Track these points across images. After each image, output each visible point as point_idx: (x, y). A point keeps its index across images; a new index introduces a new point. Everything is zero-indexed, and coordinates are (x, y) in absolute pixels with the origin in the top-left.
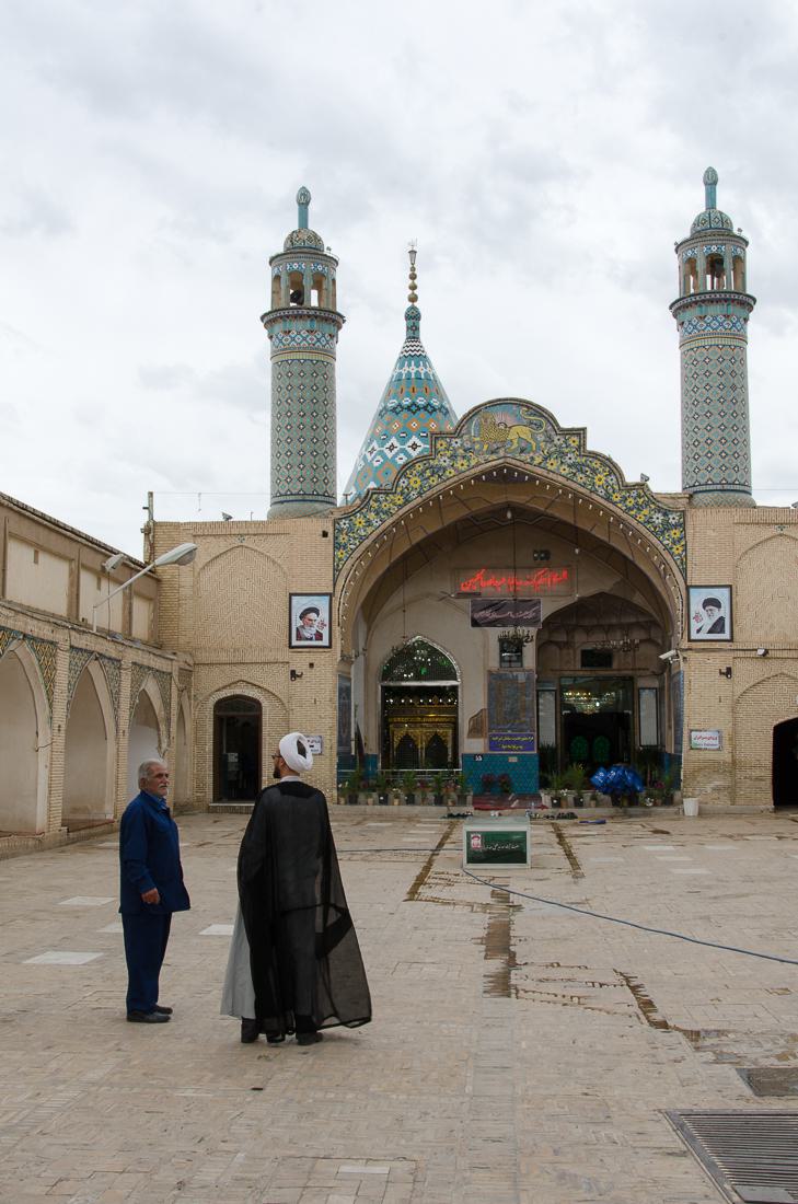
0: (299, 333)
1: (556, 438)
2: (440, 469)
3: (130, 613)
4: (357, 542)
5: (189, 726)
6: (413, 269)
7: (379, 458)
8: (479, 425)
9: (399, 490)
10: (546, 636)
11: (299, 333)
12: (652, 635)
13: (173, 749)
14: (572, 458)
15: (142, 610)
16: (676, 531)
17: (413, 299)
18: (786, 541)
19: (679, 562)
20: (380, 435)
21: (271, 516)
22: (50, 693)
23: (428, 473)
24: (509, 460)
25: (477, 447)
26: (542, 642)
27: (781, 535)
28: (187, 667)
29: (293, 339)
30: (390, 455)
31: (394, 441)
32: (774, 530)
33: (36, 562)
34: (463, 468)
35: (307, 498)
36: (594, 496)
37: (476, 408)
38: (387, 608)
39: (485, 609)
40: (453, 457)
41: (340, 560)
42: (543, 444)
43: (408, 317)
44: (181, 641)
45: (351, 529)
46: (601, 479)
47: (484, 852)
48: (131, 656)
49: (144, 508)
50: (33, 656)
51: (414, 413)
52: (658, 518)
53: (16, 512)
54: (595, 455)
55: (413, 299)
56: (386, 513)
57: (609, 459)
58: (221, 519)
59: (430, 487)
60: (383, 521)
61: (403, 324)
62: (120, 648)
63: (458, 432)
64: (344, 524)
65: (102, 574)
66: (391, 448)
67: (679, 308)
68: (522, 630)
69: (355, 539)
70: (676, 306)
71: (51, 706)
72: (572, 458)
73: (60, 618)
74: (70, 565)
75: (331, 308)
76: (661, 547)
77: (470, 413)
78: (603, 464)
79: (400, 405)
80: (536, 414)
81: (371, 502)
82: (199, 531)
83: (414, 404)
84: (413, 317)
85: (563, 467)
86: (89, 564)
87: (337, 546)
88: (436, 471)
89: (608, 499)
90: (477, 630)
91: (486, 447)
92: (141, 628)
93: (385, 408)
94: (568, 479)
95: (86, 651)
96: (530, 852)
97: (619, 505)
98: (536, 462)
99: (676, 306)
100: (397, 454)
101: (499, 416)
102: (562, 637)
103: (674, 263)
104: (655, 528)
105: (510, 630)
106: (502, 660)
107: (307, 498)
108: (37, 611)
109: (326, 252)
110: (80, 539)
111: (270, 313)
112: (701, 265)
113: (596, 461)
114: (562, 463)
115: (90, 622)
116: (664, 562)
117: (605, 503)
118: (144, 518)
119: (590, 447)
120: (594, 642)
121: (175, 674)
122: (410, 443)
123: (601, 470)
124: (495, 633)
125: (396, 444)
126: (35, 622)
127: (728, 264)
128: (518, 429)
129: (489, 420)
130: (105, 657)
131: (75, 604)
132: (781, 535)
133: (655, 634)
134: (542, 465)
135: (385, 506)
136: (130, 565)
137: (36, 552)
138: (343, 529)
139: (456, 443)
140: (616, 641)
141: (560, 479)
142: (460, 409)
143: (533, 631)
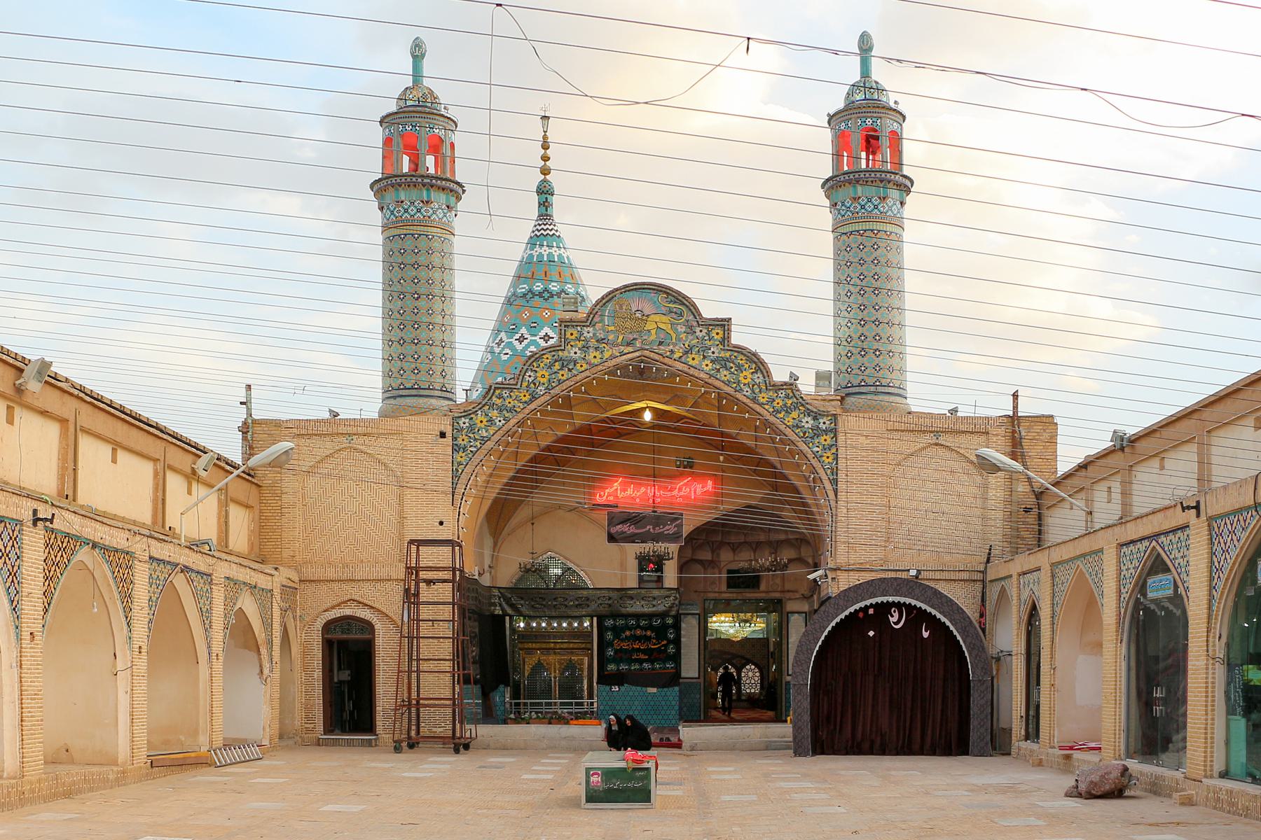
0: (869, 200)
1: (698, 330)
2: (570, 361)
3: (226, 523)
4: (478, 444)
5: (295, 649)
7: (507, 351)
8: (613, 316)
9: (525, 384)
10: (688, 554)
11: (869, 200)
12: (803, 554)
13: (277, 675)
14: (715, 351)
15: (240, 520)
16: (827, 437)
17: (545, 171)
18: (941, 451)
19: (829, 472)
20: (505, 327)
21: (383, 414)
22: (127, 610)
23: (557, 366)
24: (647, 353)
26: (683, 560)
27: (936, 444)
28: (291, 584)
29: (406, 211)
30: (519, 347)
31: (523, 330)
32: (929, 439)
33: (114, 461)
34: (596, 361)
35: (422, 392)
36: (739, 396)
37: (610, 293)
38: (514, 522)
39: (622, 523)
40: (585, 348)
41: (460, 464)
42: (683, 336)
43: (540, 192)
44: (285, 555)
45: (471, 428)
46: (747, 376)
47: (605, 791)
48: (222, 570)
49: (241, 403)
50: (106, 567)
51: (546, 300)
52: (808, 422)
53: (90, 403)
54: (740, 350)
55: (545, 171)
57: (755, 354)
58: (327, 415)
59: (560, 382)
60: (507, 420)
61: (535, 199)
62: (210, 560)
63: (590, 320)
64: (464, 423)
65: (192, 476)
67: (832, 185)
68: (661, 547)
69: (476, 440)
70: (829, 184)
71: (128, 624)
72: (715, 351)
73: (143, 525)
74: (155, 465)
75: (448, 176)
76: (810, 456)
77: (603, 298)
78: (750, 360)
79: (530, 291)
80: (678, 302)
81: (494, 399)
82: (305, 430)
83: (546, 290)
84: (545, 192)
85: (707, 362)
86: (177, 465)
87: (456, 448)
88: (566, 363)
89: (754, 400)
90: (613, 546)
91: (621, 338)
92: (240, 538)
93: (514, 294)
94: (711, 376)
95: (169, 563)
96: (657, 792)
97: (766, 407)
98: (676, 356)
99: (829, 184)
100: (528, 346)
101: (636, 303)
102: (706, 555)
103: (825, 139)
104: (805, 433)
105: (648, 547)
107: (422, 392)
108: (115, 517)
109: (443, 112)
110: (165, 437)
111: (380, 180)
112: (857, 139)
113: (741, 357)
114: (704, 357)
115: (178, 531)
116: (814, 471)
118: (242, 413)
119: (736, 339)
120: (742, 560)
121: (277, 592)
122: (542, 334)
123: (747, 366)
124: (633, 549)
126: (107, 528)
127: (885, 142)
128: (657, 318)
129: (624, 307)
130: (192, 570)
131: (160, 511)
132: (936, 444)
133: (806, 552)
134: (683, 359)
135: (511, 403)
136: (223, 465)
137: (114, 450)
138: (462, 429)
139: (588, 332)
140: (765, 560)
141: (702, 375)
142: (594, 294)
143: (673, 548)
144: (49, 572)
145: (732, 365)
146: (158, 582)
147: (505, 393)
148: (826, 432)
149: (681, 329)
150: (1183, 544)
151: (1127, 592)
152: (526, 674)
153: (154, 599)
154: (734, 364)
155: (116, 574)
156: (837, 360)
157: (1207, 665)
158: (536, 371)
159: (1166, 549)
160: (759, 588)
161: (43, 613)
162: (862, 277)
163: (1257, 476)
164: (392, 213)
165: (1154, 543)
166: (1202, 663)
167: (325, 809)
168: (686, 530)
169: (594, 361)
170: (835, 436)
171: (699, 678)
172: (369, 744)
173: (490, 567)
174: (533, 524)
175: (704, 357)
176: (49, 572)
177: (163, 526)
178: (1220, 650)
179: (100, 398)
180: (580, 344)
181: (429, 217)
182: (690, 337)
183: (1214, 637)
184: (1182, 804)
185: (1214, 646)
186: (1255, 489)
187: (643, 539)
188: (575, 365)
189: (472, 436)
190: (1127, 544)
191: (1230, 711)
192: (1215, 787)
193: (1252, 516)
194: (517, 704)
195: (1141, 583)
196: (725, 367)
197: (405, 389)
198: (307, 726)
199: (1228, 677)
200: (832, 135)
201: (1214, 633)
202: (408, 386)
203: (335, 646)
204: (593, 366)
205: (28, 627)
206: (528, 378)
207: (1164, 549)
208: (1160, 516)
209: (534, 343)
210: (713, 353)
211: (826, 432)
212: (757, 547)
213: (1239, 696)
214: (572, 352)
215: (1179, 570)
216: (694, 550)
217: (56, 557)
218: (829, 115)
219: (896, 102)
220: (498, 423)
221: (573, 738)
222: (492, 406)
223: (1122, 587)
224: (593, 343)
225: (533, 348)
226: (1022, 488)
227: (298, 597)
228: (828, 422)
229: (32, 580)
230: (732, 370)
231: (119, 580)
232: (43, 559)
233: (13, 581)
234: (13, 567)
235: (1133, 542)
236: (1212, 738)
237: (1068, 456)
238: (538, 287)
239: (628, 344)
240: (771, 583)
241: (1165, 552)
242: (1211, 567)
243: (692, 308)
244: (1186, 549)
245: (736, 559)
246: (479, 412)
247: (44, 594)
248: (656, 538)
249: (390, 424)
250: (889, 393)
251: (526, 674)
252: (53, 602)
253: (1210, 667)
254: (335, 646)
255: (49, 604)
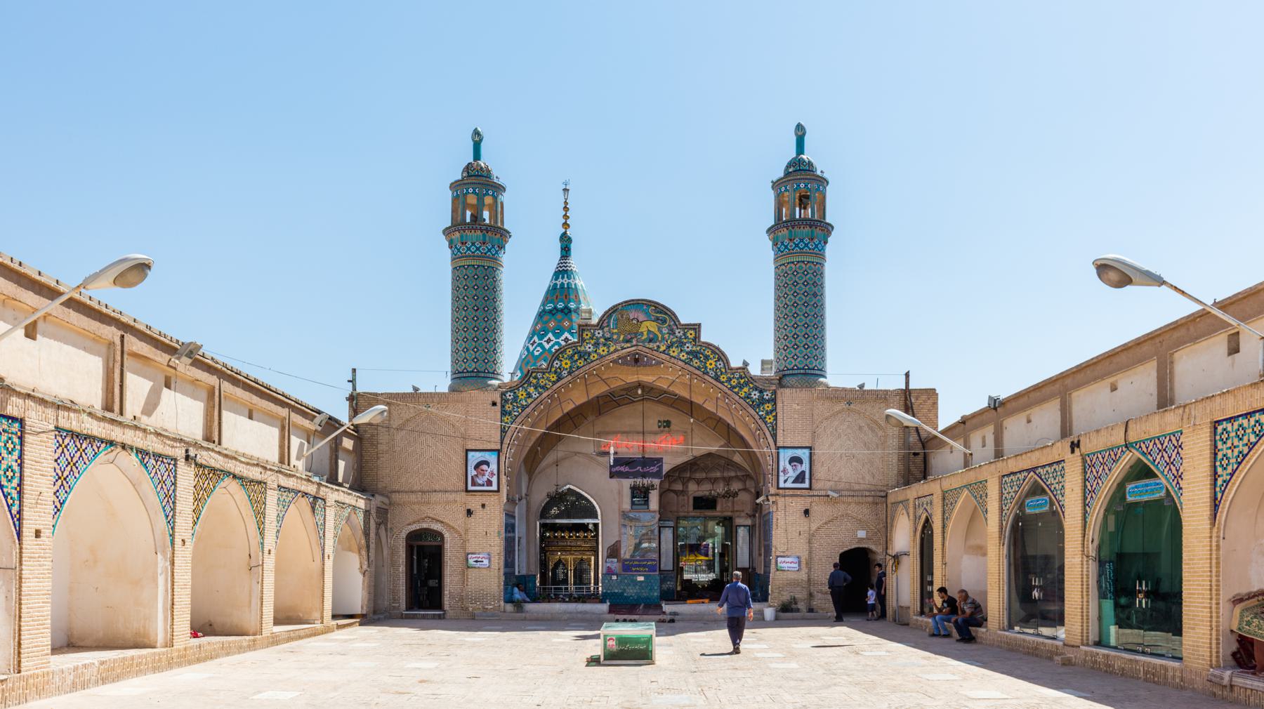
1: (677, 331)
6: (566, 203)
7: (538, 348)
10: (666, 486)
11: (802, 240)
12: (748, 486)
14: (689, 347)
16: (769, 405)
17: (566, 225)
19: (770, 429)
20: (538, 331)
21: (453, 389)
23: (576, 357)
25: (615, 337)
28: (384, 507)
29: (469, 249)
30: (547, 346)
31: (550, 335)
34: (604, 354)
38: (544, 464)
40: (596, 345)
42: (666, 336)
49: (349, 381)
54: (708, 345)
55: (566, 225)
56: (543, 387)
59: (578, 368)
60: (540, 394)
66: (549, 341)
69: (518, 407)
77: (609, 310)
80: (662, 313)
81: (531, 379)
84: (566, 209)
87: (504, 413)
88: (584, 355)
90: (615, 481)
93: (544, 311)
97: (726, 384)
98: (661, 350)
100: (553, 346)
102: (679, 487)
103: (770, 197)
105: (639, 481)
106: (633, 503)
114: (681, 351)
117: (714, 382)
118: (348, 389)
119: (703, 338)
120: (704, 490)
122: (563, 337)
123: (712, 356)
124: (627, 483)
125: (552, 338)
128: (648, 323)
129: (624, 316)
138: (508, 400)
144: (198, 495)
145: (701, 356)
146: (284, 503)
147: (539, 375)
148: (768, 401)
149: (665, 331)
150: (1059, 473)
151: (1008, 510)
152: (550, 568)
153: (281, 515)
154: (702, 354)
155: (251, 497)
156: (777, 350)
157: (1082, 561)
158: (561, 360)
159: (1043, 477)
160: (716, 509)
161: (192, 525)
162: (795, 294)
163: (1127, 422)
164: (458, 250)
165: (1032, 473)
166: (1078, 560)
167: (409, 666)
168: (666, 468)
169: (602, 353)
170: (775, 404)
171: (673, 570)
172: (440, 617)
173: (526, 495)
174: (557, 465)
175: (681, 351)
176: (198, 495)
177: (289, 465)
178: (1092, 550)
179: (238, 372)
180: (593, 342)
181: (485, 254)
182: (672, 337)
183: (1088, 541)
184: (1064, 664)
185: (1088, 548)
186: (1126, 431)
187: (635, 475)
188: (589, 356)
189: (515, 404)
190: (1008, 475)
191: (1102, 596)
192: (1092, 652)
193: (1122, 451)
194: (544, 589)
195: (1020, 503)
196: (696, 357)
197: (468, 372)
198: (393, 605)
199: (1099, 570)
200: (775, 197)
201: (1088, 538)
202: (469, 370)
203: (415, 549)
204: (602, 357)
205: (179, 535)
206: (555, 365)
207: (1041, 478)
208: (1037, 454)
209: (557, 343)
210: (688, 347)
211: (768, 401)
212: (715, 481)
213: (1110, 584)
214: (587, 347)
215: (1055, 493)
216: (670, 483)
217: (204, 484)
218: (772, 182)
219: (822, 172)
220: (534, 396)
221: (585, 613)
222: (530, 384)
223: (1004, 506)
224: (602, 340)
225: (557, 347)
226: (913, 438)
227: (389, 516)
228: (770, 395)
229: (184, 501)
230: (702, 359)
231: (254, 502)
232: (193, 485)
233: (168, 501)
234: (168, 491)
235: (1014, 473)
236: (1087, 616)
237: (947, 416)
238: (560, 305)
239: (628, 341)
240: (724, 506)
241: (1042, 480)
242: (1085, 490)
243: (673, 317)
244: (1060, 477)
245: (700, 489)
246: (521, 389)
247: (194, 511)
248: (644, 476)
249: (456, 396)
250: (813, 374)
251: (550, 568)
252: (201, 517)
253: (1085, 563)
254: (415, 549)
255: (197, 519)
